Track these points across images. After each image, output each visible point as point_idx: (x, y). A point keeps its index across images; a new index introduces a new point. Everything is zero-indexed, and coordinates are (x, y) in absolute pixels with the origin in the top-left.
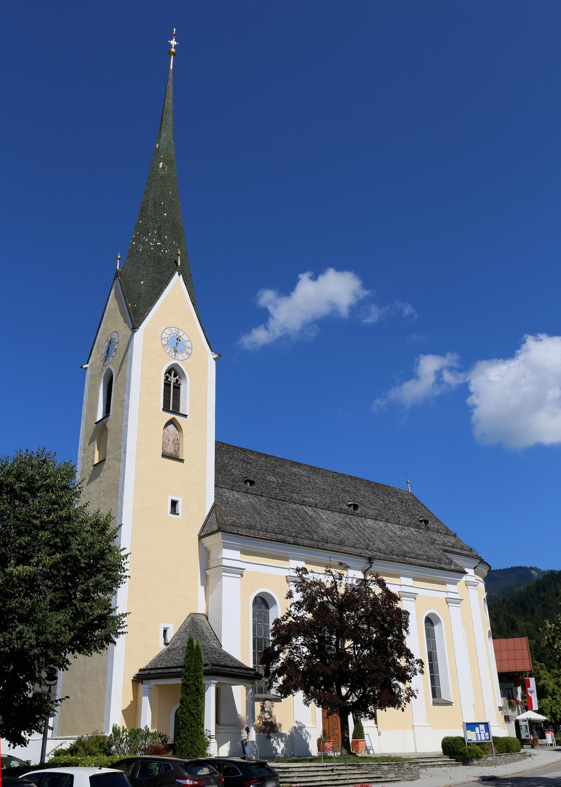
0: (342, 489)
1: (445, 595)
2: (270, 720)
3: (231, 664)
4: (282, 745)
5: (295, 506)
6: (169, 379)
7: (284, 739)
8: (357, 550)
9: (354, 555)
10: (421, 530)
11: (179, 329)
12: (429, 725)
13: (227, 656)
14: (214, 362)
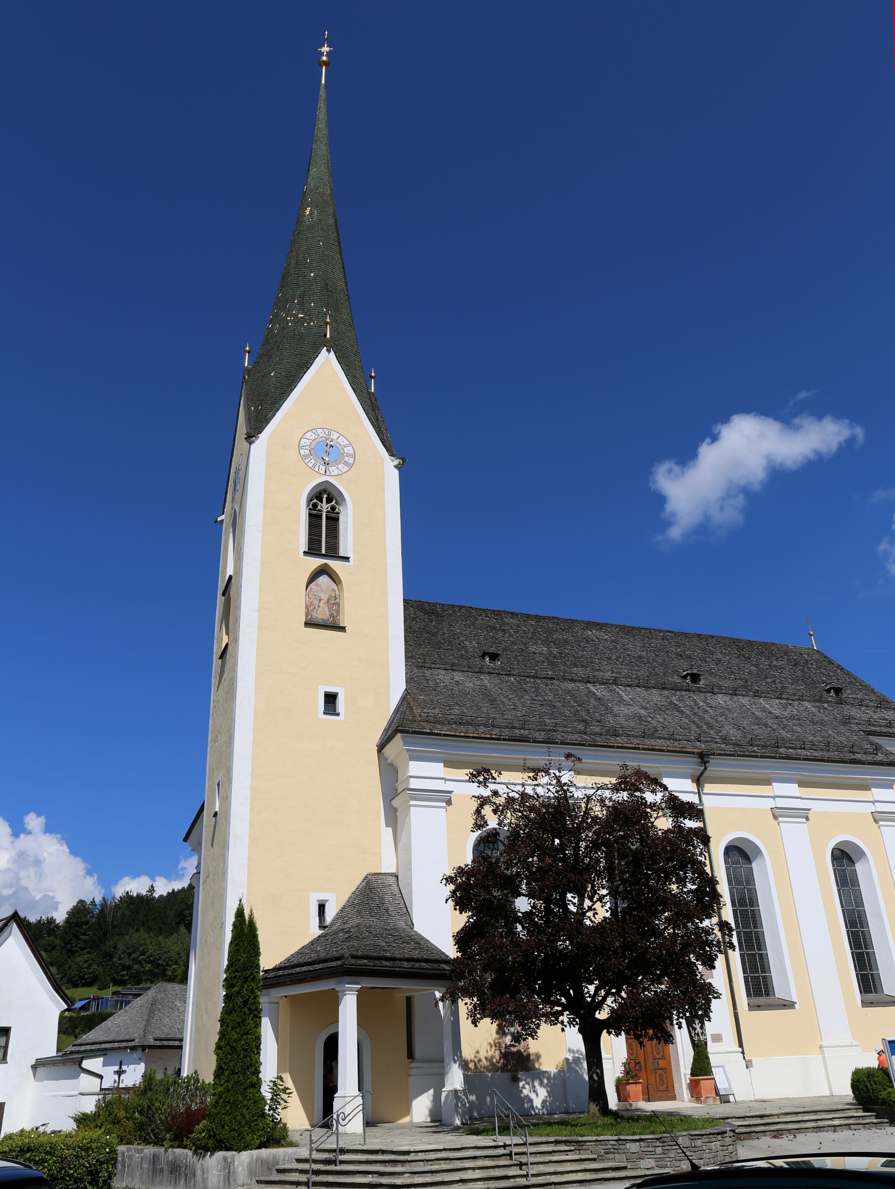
0: (677, 654)
1: (871, 808)
2: (515, 1049)
3: (416, 954)
4: (543, 1093)
5: (570, 686)
6: (319, 507)
7: (545, 1081)
8: (676, 744)
9: (669, 751)
10: (826, 705)
11: (330, 430)
12: (855, 1043)
13: (419, 942)
14: (396, 472)
